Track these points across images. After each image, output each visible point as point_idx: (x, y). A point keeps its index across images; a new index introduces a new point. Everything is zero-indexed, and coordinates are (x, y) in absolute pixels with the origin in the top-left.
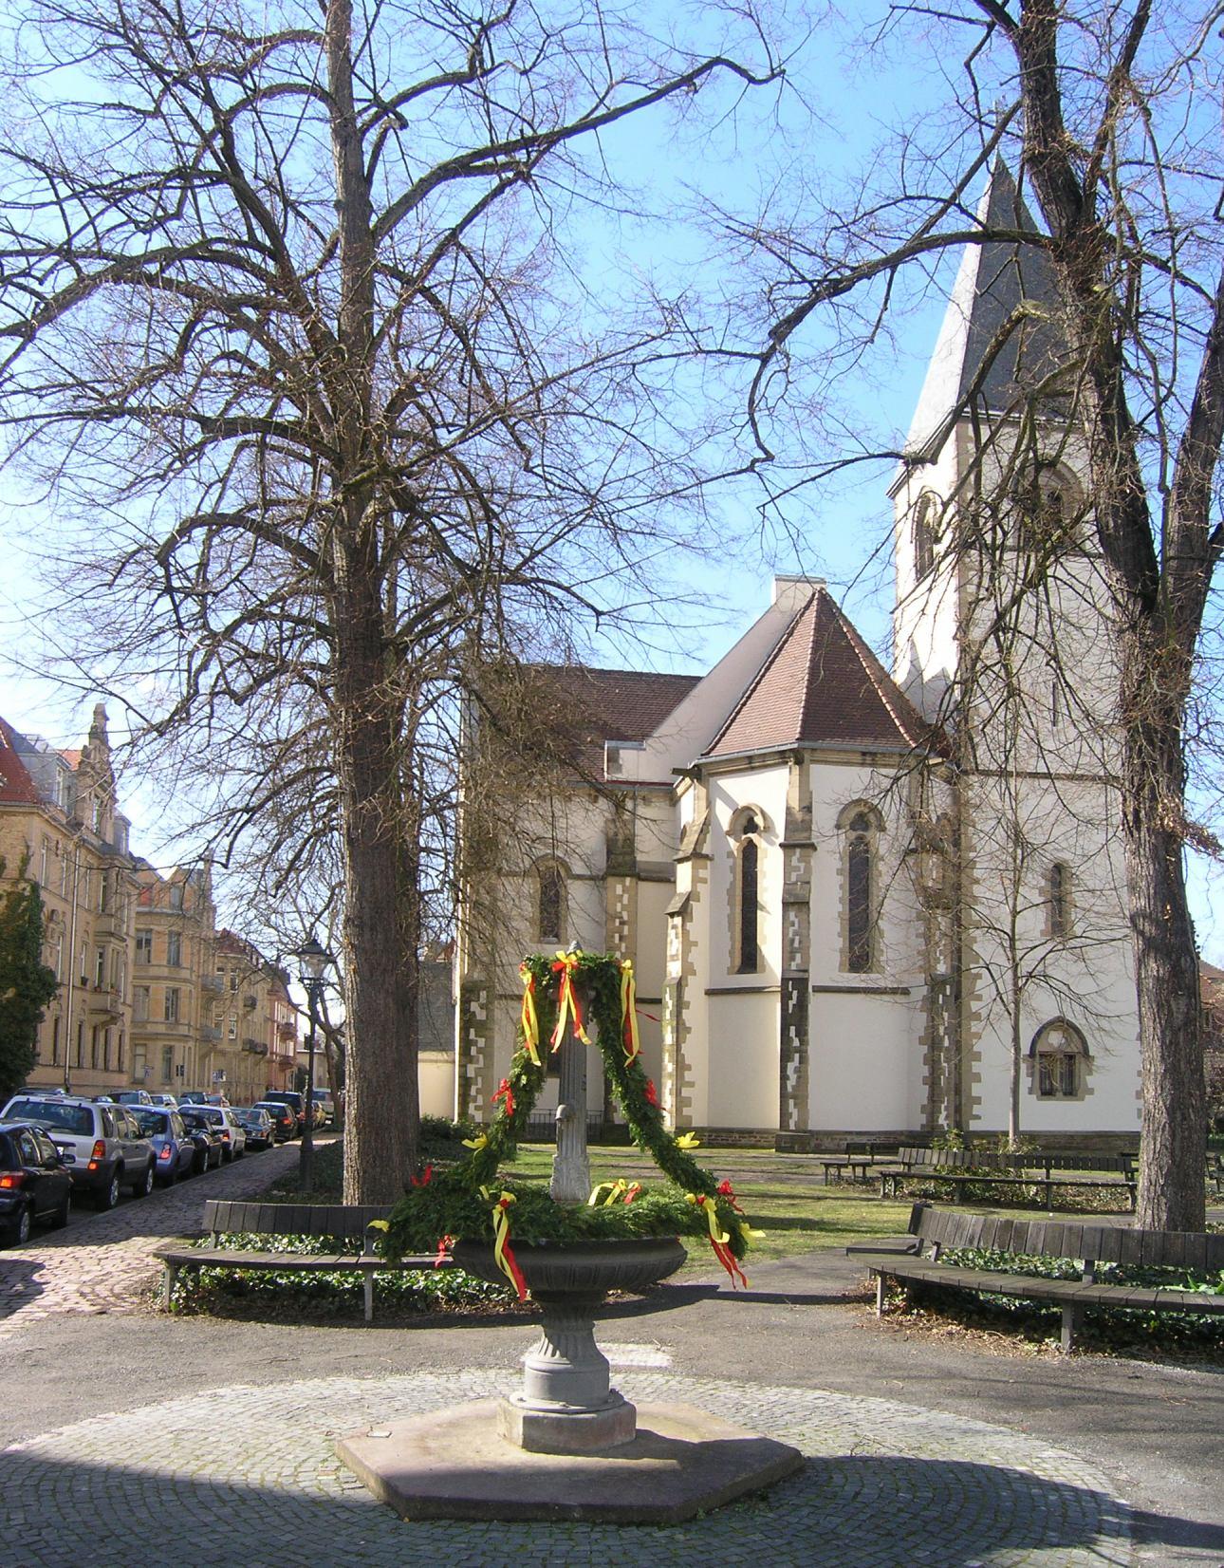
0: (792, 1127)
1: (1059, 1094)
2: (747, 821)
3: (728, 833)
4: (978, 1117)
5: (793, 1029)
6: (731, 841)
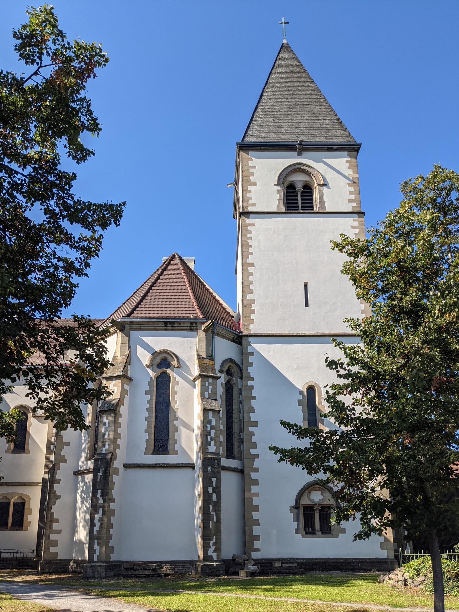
0: (96, 559)
2: (163, 361)
3: (148, 366)
4: (258, 550)
5: (99, 491)
6: (150, 371)
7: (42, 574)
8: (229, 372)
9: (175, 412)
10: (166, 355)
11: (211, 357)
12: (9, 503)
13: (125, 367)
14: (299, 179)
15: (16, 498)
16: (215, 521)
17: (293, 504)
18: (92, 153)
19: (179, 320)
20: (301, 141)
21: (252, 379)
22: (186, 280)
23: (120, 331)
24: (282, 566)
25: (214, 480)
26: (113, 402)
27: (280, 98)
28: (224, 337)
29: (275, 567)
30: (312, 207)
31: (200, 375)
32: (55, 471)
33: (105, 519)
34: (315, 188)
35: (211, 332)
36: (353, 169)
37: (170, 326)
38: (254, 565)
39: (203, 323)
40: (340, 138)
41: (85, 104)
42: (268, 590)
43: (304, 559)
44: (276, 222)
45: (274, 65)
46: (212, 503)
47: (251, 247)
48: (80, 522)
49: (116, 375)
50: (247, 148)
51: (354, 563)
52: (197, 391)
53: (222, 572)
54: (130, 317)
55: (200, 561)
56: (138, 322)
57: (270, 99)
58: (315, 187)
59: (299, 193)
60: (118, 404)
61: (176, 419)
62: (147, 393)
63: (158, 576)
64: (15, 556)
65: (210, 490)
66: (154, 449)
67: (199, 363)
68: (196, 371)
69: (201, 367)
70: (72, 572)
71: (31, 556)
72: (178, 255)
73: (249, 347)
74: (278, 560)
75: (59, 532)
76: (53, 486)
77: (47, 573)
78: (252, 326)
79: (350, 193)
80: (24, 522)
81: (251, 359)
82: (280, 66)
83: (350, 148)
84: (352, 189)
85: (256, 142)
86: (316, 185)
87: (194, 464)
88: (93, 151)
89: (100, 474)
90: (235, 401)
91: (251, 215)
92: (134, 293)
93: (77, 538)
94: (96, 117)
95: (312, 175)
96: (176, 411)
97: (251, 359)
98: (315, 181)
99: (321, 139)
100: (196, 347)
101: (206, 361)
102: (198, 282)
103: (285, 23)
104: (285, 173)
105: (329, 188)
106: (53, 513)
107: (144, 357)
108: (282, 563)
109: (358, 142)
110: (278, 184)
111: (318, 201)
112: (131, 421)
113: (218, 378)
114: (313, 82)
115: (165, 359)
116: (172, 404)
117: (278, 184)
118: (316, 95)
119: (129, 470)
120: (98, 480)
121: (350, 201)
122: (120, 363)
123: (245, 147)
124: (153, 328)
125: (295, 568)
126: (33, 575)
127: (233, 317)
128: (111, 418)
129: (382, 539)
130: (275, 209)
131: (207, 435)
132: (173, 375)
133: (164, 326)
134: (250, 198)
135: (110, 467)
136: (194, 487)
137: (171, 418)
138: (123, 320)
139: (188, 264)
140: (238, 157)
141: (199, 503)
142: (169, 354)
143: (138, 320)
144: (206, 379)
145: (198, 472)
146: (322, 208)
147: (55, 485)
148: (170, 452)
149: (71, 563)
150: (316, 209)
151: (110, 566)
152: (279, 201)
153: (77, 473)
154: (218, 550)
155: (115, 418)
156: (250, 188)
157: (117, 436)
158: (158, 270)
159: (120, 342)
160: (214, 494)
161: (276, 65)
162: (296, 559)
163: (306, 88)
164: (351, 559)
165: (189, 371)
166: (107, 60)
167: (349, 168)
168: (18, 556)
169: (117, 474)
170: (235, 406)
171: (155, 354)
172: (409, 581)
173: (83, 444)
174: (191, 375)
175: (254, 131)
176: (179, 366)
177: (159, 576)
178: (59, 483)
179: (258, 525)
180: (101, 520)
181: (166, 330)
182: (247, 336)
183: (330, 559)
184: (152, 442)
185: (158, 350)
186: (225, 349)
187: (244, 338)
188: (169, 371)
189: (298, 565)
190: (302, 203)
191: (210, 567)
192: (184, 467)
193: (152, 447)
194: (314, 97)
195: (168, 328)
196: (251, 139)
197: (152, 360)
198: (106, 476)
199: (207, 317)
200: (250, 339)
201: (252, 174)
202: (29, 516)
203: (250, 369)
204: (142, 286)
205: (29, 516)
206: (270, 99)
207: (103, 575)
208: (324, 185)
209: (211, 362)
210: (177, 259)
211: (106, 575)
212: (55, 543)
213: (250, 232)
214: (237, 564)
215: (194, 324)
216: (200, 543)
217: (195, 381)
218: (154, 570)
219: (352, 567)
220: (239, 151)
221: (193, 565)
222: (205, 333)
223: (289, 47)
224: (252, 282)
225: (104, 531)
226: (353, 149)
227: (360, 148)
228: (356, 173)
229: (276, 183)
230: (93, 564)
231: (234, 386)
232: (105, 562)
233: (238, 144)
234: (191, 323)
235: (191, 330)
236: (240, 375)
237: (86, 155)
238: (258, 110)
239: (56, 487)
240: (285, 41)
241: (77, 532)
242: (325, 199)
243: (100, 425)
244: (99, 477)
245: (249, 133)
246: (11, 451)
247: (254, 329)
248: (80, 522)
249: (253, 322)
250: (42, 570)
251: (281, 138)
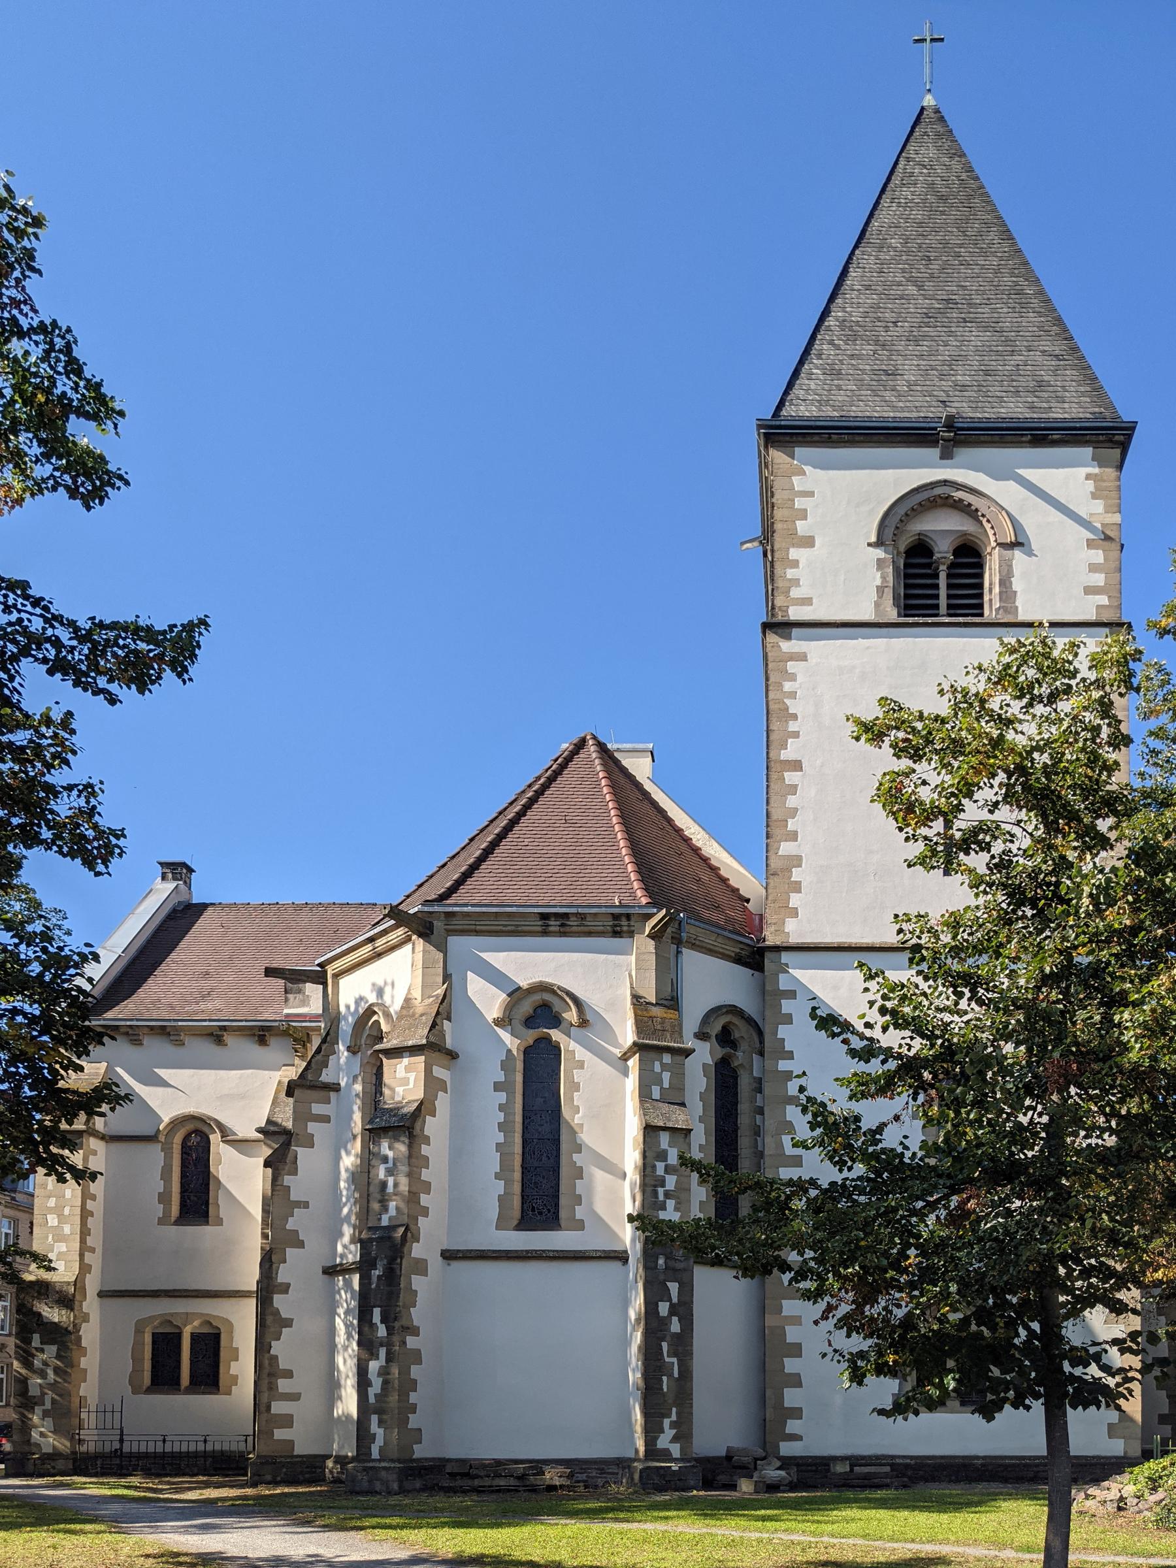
0: (375, 1454)
2: (540, 1010)
3: (497, 1022)
5: (377, 1314)
6: (505, 1036)
7: (254, 1485)
8: (726, 1038)
9: (574, 1133)
10: (547, 997)
11: (671, 1000)
12: (179, 1336)
13: (434, 1025)
14: (943, 528)
15: (196, 1323)
16: (676, 1375)
18: (120, 478)
19: (580, 910)
20: (950, 418)
21: (790, 1056)
22: (611, 805)
23: (420, 935)
24: (852, 1470)
25: (674, 1287)
26: (405, 1110)
27: (899, 284)
28: (710, 952)
29: (835, 1474)
30: (981, 606)
31: (635, 1044)
32: (274, 1266)
33: (395, 1371)
34: (990, 554)
35: (671, 939)
36: (1105, 498)
37: (556, 924)
38: (779, 1469)
39: (649, 916)
40: (1072, 407)
41: (59, 343)
42: (764, 1519)
43: (911, 1458)
44: (868, 648)
45: (889, 179)
46: (668, 1338)
47: (795, 717)
48: (347, 1376)
49: (410, 1043)
50: (788, 439)
51: (1037, 1465)
52: (631, 1083)
53: (692, 1483)
54: (448, 902)
55: (638, 1460)
56: (467, 914)
57: (868, 287)
58: (989, 550)
59: (942, 567)
60: (418, 1113)
61: (578, 1148)
62: (498, 1087)
63: (529, 1491)
64: (201, 1447)
65: (663, 1308)
66: (522, 1216)
67: (636, 1015)
68: (628, 1035)
69: (641, 1025)
70: (331, 1482)
71: (242, 1447)
72: (594, 738)
73: (781, 976)
74: (844, 1459)
75: (295, 1397)
76: (272, 1299)
77: (269, 1483)
78: (791, 925)
79: (1093, 568)
80: (221, 1376)
81: (787, 1006)
82: (910, 180)
83: (1101, 438)
84: (1098, 556)
85: (817, 419)
86: (993, 544)
87: (626, 1252)
88: (122, 472)
89: (376, 1273)
90: (744, 1107)
91: (795, 631)
92: (472, 840)
93: (340, 1412)
94: (97, 380)
95: (983, 516)
96: (577, 1129)
97: (787, 1006)
98: (990, 532)
99: (1014, 409)
100: (630, 976)
101: (657, 1012)
102: (652, 812)
103: (932, 40)
104: (901, 511)
105: (1030, 553)
106: (277, 1357)
107: (490, 1002)
108: (852, 1466)
109: (1127, 417)
110: (879, 543)
111: (996, 590)
112: (458, 1152)
113: (688, 1053)
114: (1007, 234)
115: (545, 1006)
116: (566, 1112)
117: (879, 543)
118: (1012, 275)
119: (457, 1265)
120: (373, 1286)
121: (1089, 590)
122: (422, 1015)
123: (781, 434)
124: (509, 928)
125: (886, 1475)
126: (232, 1487)
127: (748, 901)
128: (402, 1148)
129: (1113, 1416)
130: (867, 614)
131: (655, 1186)
132: (570, 1046)
133: (540, 923)
134: (796, 582)
135: (402, 1258)
136: (626, 1303)
137: (564, 1147)
138: (426, 909)
139: (627, 762)
141: (638, 1338)
142: (554, 992)
143: (465, 909)
144: (652, 1055)
145: (635, 1268)
146: (1006, 610)
147: (276, 1297)
148: (563, 1223)
149: (330, 1464)
150: (989, 614)
151: (411, 1468)
152: (880, 590)
153: (332, 1271)
154: (683, 1435)
155: (410, 1146)
157: (418, 1187)
158: (538, 778)
160: (675, 1319)
161: (896, 180)
162: (893, 1457)
163: (984, 253)
164: (1030, 1458)
165: (608, 1031)
166: (38, 222)
167: (1094, 496)
168: (209, 1447)
169: (424, 1273)
170: (744, 1120)
171: (516, 994)
172: (1131, 1501)
173: (345, 1204)
174: (616, 1044)
175: (813, 387)
176: (584, 1023)
177: (534, 1491)
178: (286, 1292)
179: (800, 1385)
180: (384, 1372)
181: (545, 933)
182: (778, 949)
183: (977, 1457)
184: (517, 1201)
185: (524, 984)
186: (710, 982)
187: (768, 956)
188: (556, 1035)
189: (892, 1470)
190: (949, 597)
191: (662, 1472)
192: (600, 1258)
193: (516, 1212)
194: (1008, 280)
195: (551, 929)
196: (801, 409)
197: (509, 1008)
198: (392, 1277)
199: (656, 903)
200: (785, 957)
201: (803, 514)
202: (232, 1363)
203: (783, 1031)
204: (491, 821)
205: (232, 1363)
206: (868, 287)
207: (395, 1486)
208: (1016, 544)
209: (671, 1014)
210: (592, 749)
211: (400, 1487)
212: (287, 1421)
213: (793, 678)
214: (735, 1467)
215: (624, 919)
216: (639, 1422)
217: (626, 1060)
218: (522, 1478)
219: (1031, 1475)
220: (766, 447)
221: (624, 1468)
222: (653, 942)
223: (942, 119)
224: (794, 812)
225: (393, 1398)
226: (1111, 441)
227: (1130, 437)
228: (1116, 509)
229: (873, 539)
230: (371, 1464)
231: (741, 1072)
232: (399, 1461)
233: (759, 427)
234: (616, 917)
235: (616, 934)
236: (758, 1045)
237: (103, 484)
238: (830, 322)
239: (278, 1300)
240: (929, 100)
241: (340, 1398)
242: (1017, 584)
243: (372, 1163)
244: (374, 1279)
245: (797, 391)
246: (173, 1219)
247: (795, 931)
248: (347, 1376)
249: (794, 913)
250: (256, 1478)
251: (894, 408)
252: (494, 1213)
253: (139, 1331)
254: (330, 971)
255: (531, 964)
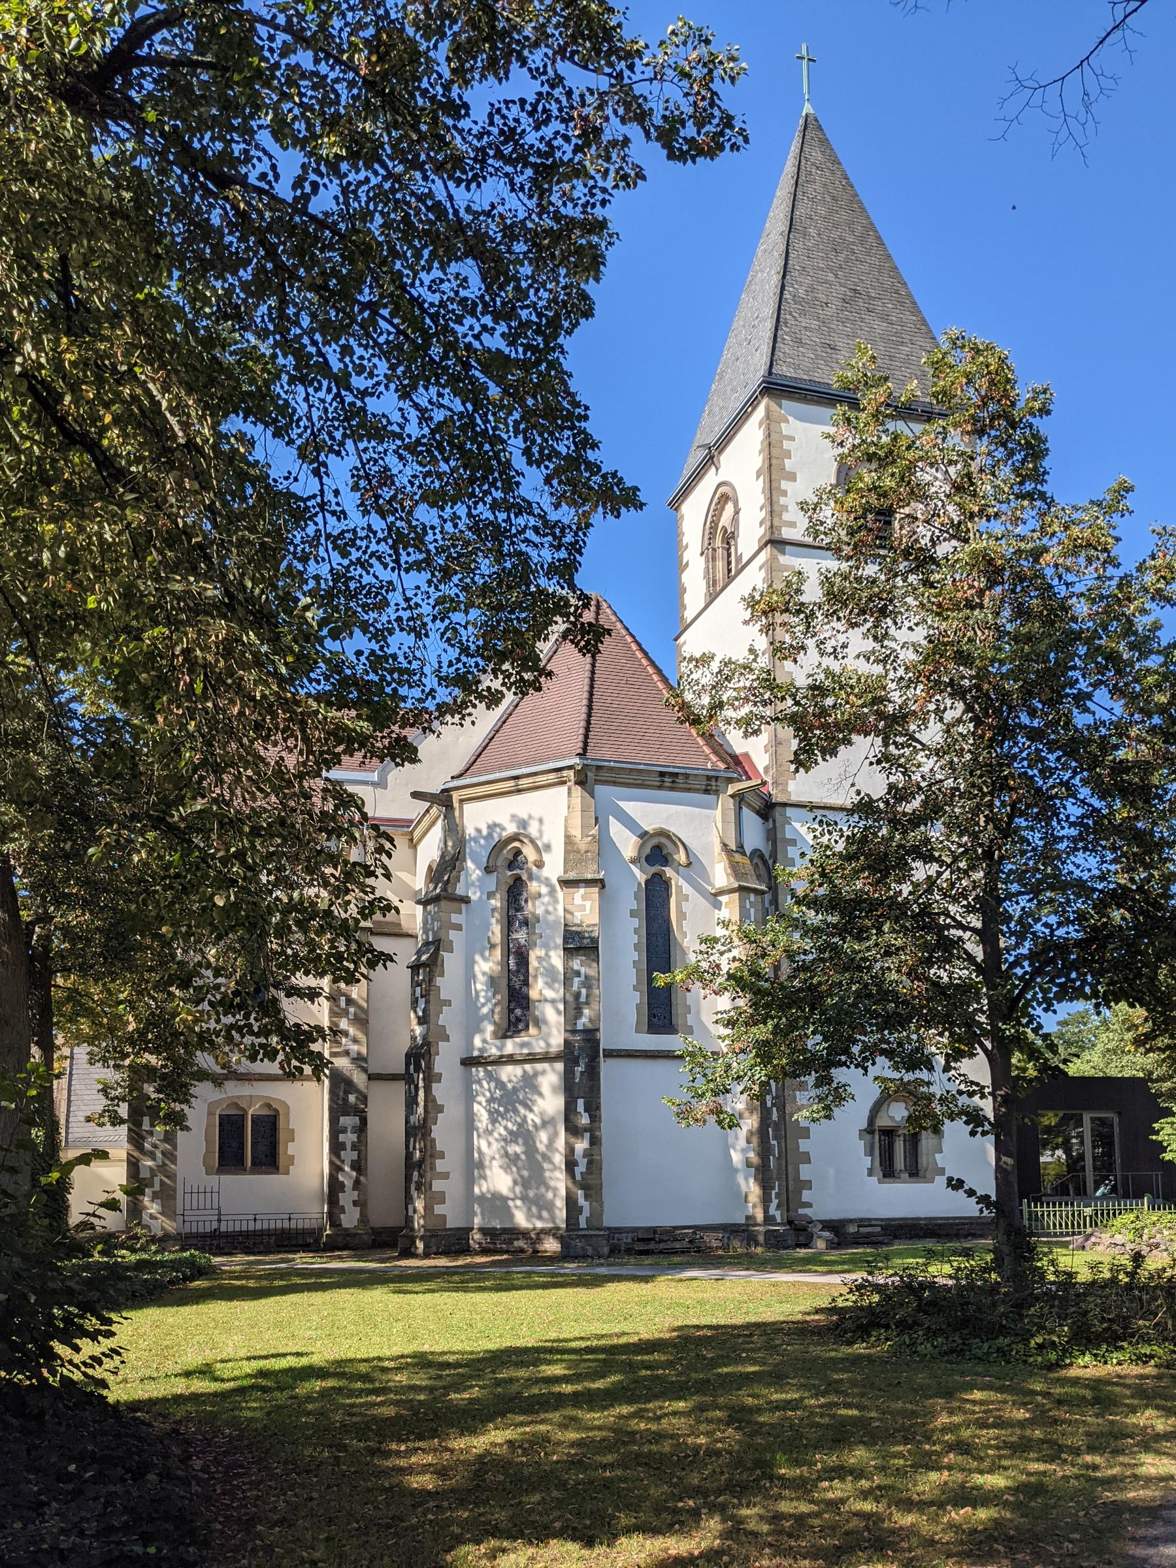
0: (583, 1224)
1: (905, 1176)
3: (633, 861)
5: (581, 1102)
10: (663, 840)
12: (243, 1117)
17: (864, 1125)
62: (633, 914)
75: (445, 1176)
89: (579, 1069)
107: (627, 845)
115: (658, 848)
132: (678, 882)
140: (753, 403)
156: (784, 485)
159: (578, 807)
161: (802, 178)
165: (705, 875)
182: (785, 805)
188: (669, 872)
200: (790, 812)
201: (788, 454)
223: (820, 128)
234: (709, 778)
235: (706, 792)
252: (633, 1018)
253: (210, 1114)
254: (456, 796)
255: (653, 813)
